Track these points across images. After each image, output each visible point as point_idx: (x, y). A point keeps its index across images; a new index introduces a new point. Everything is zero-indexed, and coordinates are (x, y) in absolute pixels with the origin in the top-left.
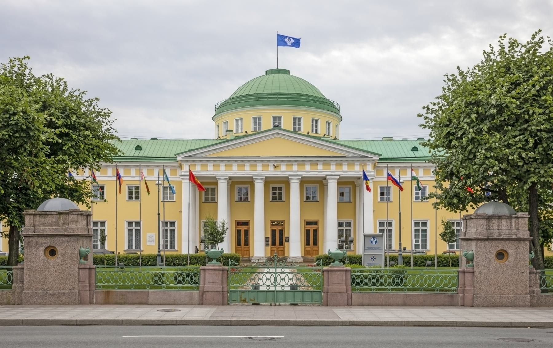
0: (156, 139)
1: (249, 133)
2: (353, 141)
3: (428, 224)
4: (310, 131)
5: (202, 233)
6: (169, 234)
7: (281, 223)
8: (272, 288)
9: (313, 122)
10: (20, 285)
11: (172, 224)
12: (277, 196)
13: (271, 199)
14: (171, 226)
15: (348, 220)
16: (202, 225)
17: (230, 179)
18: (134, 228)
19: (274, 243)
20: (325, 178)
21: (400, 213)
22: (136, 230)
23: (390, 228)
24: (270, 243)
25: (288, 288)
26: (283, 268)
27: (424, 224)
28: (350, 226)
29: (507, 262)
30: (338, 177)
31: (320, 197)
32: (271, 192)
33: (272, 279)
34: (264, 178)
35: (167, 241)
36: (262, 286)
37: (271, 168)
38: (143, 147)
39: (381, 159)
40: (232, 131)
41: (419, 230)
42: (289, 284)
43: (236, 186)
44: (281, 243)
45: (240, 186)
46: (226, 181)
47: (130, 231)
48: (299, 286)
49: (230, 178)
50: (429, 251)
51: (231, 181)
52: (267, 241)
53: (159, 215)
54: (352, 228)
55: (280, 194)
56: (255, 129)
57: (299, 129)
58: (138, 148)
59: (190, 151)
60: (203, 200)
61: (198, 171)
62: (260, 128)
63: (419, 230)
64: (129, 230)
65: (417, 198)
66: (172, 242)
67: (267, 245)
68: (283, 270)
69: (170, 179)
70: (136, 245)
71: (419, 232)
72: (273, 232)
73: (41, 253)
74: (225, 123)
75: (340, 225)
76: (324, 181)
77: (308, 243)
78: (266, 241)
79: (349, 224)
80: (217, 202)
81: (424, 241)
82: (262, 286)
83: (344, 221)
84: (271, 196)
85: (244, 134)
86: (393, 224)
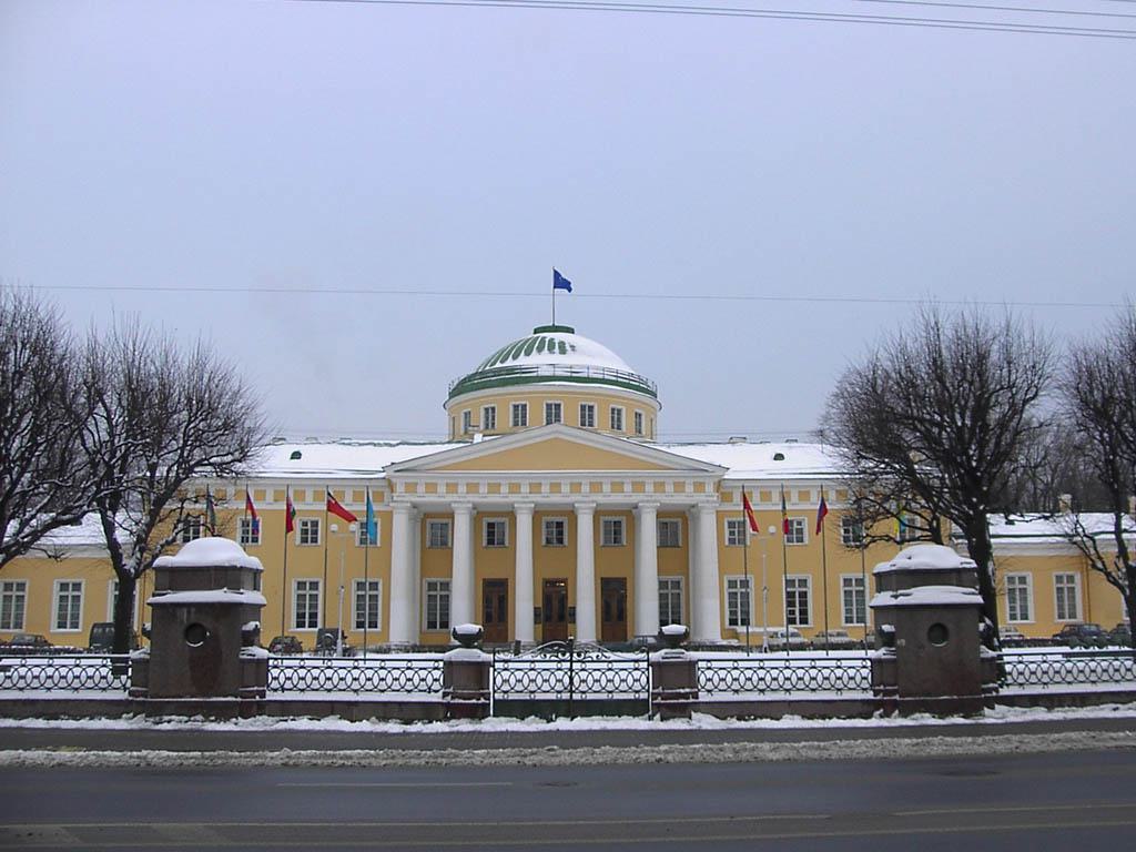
6: (307, 620)
7: (622, 582)
8: (566, 696)
9: (613, 413)
10: (765, 645)
11: (314, 585)
13: (544, 542)
14: (68, 590)
15: (676, 578)
16: (425, 586)
17: (474, 508)
19: (548, 618)
26: (24, 658)
27: (77, 586)
28: (79, 590)
33: (566, 680)
35: (793, 612)
41: (851, 592)
44: (562, 618)
47: (1060, 590)
51: (415, 511)
60: (428, 544)
63: (851, 592)
64: (441, 627)
65: (548, 541)
66: (374, 615)
68: (24, 662)
69: (255, 507)
71: (851, 596)
72: (547, 599)
74: (466, 414)
76: (634, 511)
78: (574, 614)
79: (677, 584)
80: (452, 548)
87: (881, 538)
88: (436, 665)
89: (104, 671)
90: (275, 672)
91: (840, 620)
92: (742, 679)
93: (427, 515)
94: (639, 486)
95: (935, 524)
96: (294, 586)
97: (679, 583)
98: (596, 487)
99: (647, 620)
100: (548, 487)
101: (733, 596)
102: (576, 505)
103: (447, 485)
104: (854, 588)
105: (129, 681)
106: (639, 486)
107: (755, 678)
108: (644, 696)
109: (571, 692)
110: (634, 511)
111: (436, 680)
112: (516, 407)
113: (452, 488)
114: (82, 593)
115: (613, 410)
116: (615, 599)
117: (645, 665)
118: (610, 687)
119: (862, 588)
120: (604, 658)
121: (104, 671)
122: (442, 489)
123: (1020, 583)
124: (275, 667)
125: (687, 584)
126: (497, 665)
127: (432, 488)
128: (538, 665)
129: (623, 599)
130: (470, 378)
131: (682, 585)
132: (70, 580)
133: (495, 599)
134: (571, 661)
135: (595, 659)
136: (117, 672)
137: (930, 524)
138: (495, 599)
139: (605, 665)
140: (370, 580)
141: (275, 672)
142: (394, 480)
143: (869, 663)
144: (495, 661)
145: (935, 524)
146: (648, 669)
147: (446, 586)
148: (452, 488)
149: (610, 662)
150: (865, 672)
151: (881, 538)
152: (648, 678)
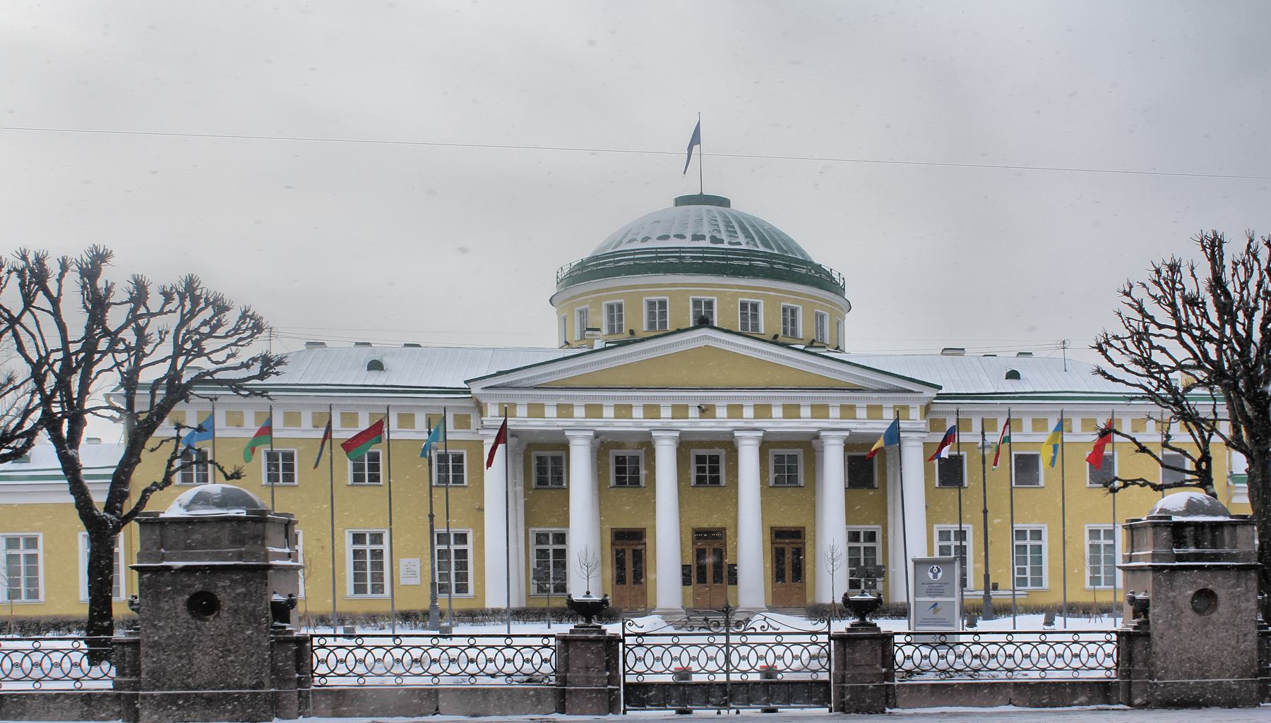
0: (418, 346)
1: (639, 336)
2: (867, 356)
3: (1045, 535)
4: (781, 333)
5: (533, 554)
7: (797, 534)
8: (721, 678)
11: (377, 538)
12: (707, 474)
13: (693, 481)
18: (1103, 542)
20: (816, 436)
21: (985, 512)
22: (555, 550)
23: (1038, 543)
24: (694, 579)
25: (755, 677)
26: (36, 640)
27: (32, 542)
29: (1215, 615)
30: (847, 434)
31: (805, 478)
32: (534, 463)
34: (677, 434)
35: (1023, 571)
36: (696, 672)
37: (693, 413)
38: (386, 361)
39: (940, 397)
40: (598, 330)
42: (672, 669)
43: (771, 451)
45: (780, 452)
46: (587, 442)
48: (780, 672)
49: (597, 435)
50: (1045, 591)
52: (686, 570)
53: (431, 516)
54: (878, 545)
55: (715, 470)
56: (652, 326)
57: (755, 327)
58: (375, 366)
59: (500, 373)
60: (772, 482)
61: (521, 420)
62: (663, 324)
66: (462, 577)
67: (686, 581)
70: (373, 586)
71: (1099, 552)
73: (181, 607)
75: (854, 537)
76: (814, 442)
77: (779, 575)
79: (871, 536)
80: (567, 489)
81: (1038, 571)
82: (696, 672)
83: (862, 528)
84: (693, 474)
85: (625, 335)
86: (969, 535)
87: (1134, 482)
88: (546, 641)
89: (76, 657)
90: (322, 653)
91: (1084, 582)
92: (1018, 655)
93: (531, 446)
94: (565, 410)
95: (1204, 465)
96: (349, 539)
97: (538, 535)
98: (680, 411)
99: (831, 580)
100: (781, 410)
101: (542, 554)
102: (736, 434)
103: (784, 407)
105: (114, 669)
106: (820, 410)
107: (1068, 654)
108: (824, 676)
109: (727, 672)
110: (814, 442)
111: (545, 661)
112: (651, 304)
113: (735, 410)
114: (40, 551)
115: (785, 310)
116: (789, 553)
117: (825, 638)
118: (1076, 663)
119: (1111, 542)
120: (770, 630)
121: (76, 657)
122: (721, 412)
123: (373, 542)
124: (323, 647)
125: (885, 538)
126: (628, 640)
127: (705, 411)
128: (683, 640)
129: (639, 557)
130: (583, 265)
131: (879, 537)
132: (368, 531)
133: (628, 551)
134: (727, 635)
135: (759, 630)
136: (94, 658)
137: (1198, 464)
138: (628, 551)
139: (772, 639)
140: (453, 530)
141: (322, 653)
142: (483, 401)
143: (1114, 637)
144: (625, 635)
145: (1204, 465)
146: (829, 644)
147: (561, 538)
148: (735, 410)
149: (779, 634)
150: (1110, 648)
151: (1134, 482)
152: (625, 661)
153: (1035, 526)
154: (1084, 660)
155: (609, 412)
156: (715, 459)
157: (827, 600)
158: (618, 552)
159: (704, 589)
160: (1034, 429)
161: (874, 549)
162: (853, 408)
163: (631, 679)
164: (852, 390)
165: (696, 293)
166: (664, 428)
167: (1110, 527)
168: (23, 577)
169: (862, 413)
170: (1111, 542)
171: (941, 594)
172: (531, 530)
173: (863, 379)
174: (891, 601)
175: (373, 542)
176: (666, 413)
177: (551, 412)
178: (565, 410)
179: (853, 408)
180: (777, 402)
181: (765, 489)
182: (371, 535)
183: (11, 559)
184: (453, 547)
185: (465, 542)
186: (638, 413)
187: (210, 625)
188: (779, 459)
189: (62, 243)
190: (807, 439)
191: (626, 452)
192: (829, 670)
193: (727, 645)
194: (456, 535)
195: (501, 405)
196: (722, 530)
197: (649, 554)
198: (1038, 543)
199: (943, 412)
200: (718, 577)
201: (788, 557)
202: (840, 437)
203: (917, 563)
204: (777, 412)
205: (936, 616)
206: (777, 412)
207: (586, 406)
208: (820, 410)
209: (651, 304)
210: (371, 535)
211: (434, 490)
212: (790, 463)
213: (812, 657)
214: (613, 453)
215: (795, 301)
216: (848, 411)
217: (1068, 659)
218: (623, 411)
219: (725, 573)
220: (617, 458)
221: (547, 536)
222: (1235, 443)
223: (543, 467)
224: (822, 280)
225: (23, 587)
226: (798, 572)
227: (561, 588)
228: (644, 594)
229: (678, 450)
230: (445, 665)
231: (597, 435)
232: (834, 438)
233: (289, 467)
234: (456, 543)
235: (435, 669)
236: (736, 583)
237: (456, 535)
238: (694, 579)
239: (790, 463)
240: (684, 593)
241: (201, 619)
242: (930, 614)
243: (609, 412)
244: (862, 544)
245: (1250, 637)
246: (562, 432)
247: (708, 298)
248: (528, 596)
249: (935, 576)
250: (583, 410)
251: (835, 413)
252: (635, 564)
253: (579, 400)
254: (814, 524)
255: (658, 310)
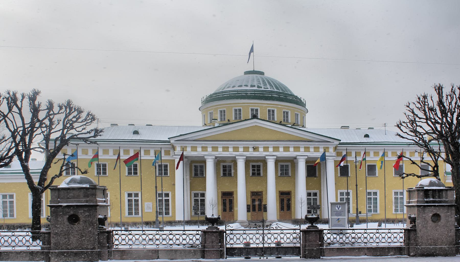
0: (151, 125)
1: (231, 122)
2: (314, 129)
3: (378, 194)
4: (283, 121)
5: (193, 201)
7: (288, 194)
8: (261, 246)
11: (136, 195)
12: (256, 172)
13: (251, 174)
18: (399, 196)
20: (295, 158)
21: (357, 185)
22: (201, 199)
23: (376, 197)
24: (251, 210)
25: (273, 245)
26: (13, 232)
27: (11, 197)
29: (440, 223)
30: (307, 157)
31: (291, 173)
32: (193, 168)
34: (245, 157)
35: (370, 207)
36: (252, 244)
37: (251, 149)
38: (140, 131)
39: (340, 144)
40: (217, 119)
42: (243, 242)
43: (279, 163)
45: (282, 164)
46: (212, 160)
48: (282, 243)
49: (216, 158)
50: (378, 214)
52: (248, 207)
53: (156, 187)
54: (318, 197)
55: (259, 170)
56: (236, 118)
57: (273, 119)
58: (136, 132)
59: (181, 135)
60: (279, 175)
61: (189, 152)
62: (240, 118)
66: (167, 209)
67: (248, 211)
70: (135, 212)
71: (398, 200)
73: (66, 220)
75: (309, 194)
76: (295, 160)
77: (282, 208)
79: (315, 194)
80: (205, 177)
81: (375, 207)
82: (252, 244)
83: (312, 191)
84: (251, 172)
85: (226, 122)
86: (351, 194)
87: (410, 175)
88: (197, 232)
89: (27, 238)
90: (116, 237)
91: (392, 211)
92: (368, 237)
93: (192, 162)
94: (204, 149)
95: (436, 169)
96: (126, 195)
97: (195, 194)
98: (246, 149)
99: (301, 210)
100: (282, 149)
101: (196, 201)
102: (267, 157)
103: (284, 147)
104: (8, 200)
105: (41, 242)
106: (297, 149)
107: (386, 237)
108: (298, 245)
109: (263, 244)
110: (295, 160)
111: (197, 239)
112: (236, 110)
113: (266, 149)
114: (14, 200)
115: (284, 112)
116: (286, 201)
117: (298, 231)
118: (389, 240)
119: (402, 196)
120: (279, 228)
121: (27, 238)
122: (261, 149)
123: (135, 196)
124: (117, 234)
125: (320, 195)
126: (227, 232)
127: (255, 149)
128: (247, 232)
129: (231, 202)
130: (211, 96)
131: (318, 195)
132: (133, 192)
133: (227, 200)
134: (263, 230)
135: (275, 228)
136: (34, 238)
137: (434, 168)
138: (227, 200)
139: (279, 231)
140: (164, 192)
141: (116, 237)
142: (175, 145)
143: (403, 231)
144: (226, 230)
145: (436, 169)
146: (300, 233)
147: (203, 195)
148: (266, 149)
149: (282, 230)
150: (402, 235)
151: (410, 175)
152: (226, 240)
153: (374, 191)
154: (392, 239)
155: (220, 149)
156: (259, 166)
157: (299, 217)
158: (224, 200)
159: (255, 213)
160: (374, 156)
161: (316, 199)
162: (309, 148)
163: (228, 246)
164: (308, 141)
165: (252, 106)
166: (240, 155)
167: (402, 191)
168: (8, 209)
169: (312, 150)
170: (402, 196)
171: (340, 215)
172: (192, 192)
173: (312, 137)
174: (322, 218)
175: (135, 196)
176: (241, 150)
177: (199, 149)
178: (204, 149)
179: (309, 148)
180: (281, 146)
181: (277, 177)
182: (134, 194)
183: (4, 203)
184: (164, 198)
185: (168, 197)
186: (231, 150)
187: (76, 226)
188: (282, 166)
189: (22, 88)
190: (292, 159)
191: (227, 164)
192: (300, 243)
193: (263, 234)
194: (165, 194)
195: (181, 147)
196: (261, 192)
197: (235, 201)
198: (376, 197)
199: (341, 149)
200: (260, 209)
201: (285, 202)
202: (304, 158)
203: (332, 204)
204: (281, 149)
205: (339, 223)
206: (281, 149)
207: (212, 147)
208: (297, 149)
209: (236, 110)
210: (134, 194)
211: (157, 177)
212: (286, 168)
213: (294, 238)
214: (222, 164)
215: (288, 109)
216: (307, 149)
217: (386, 239)
218: (226, 149)
219: (262, 208)
220: (223, 166)
221: (198, 194)
222: (447, 161)
223: (196, 169)
224: (297, 101)
225: (8, 213)
226: (289, 207)
227: (203, 213)
228: (233, 215)
229: (245, 163)
230: (161, 241)
231: (216, 158)
232: (302, 159)
233: (105, 169)
234: (165, 197)
235: (158, 242)
236: (266, 211)
237: (165, 194)
238: (251, 210)
239: (286, 168)
240: (247, 215)
241: (73, 224)
242: (336, 222)
243: (220, 149)
244: (312, 197)
245: (452, 231)
246: (204, 157)
247: (256, 108)
248: (191, 216)
249: (338, 209)
250: (211, 148)
251: (302, 150)
252: (230, 204)
253: (209, 145)
254: (295, 190)
255: (238, 112)
